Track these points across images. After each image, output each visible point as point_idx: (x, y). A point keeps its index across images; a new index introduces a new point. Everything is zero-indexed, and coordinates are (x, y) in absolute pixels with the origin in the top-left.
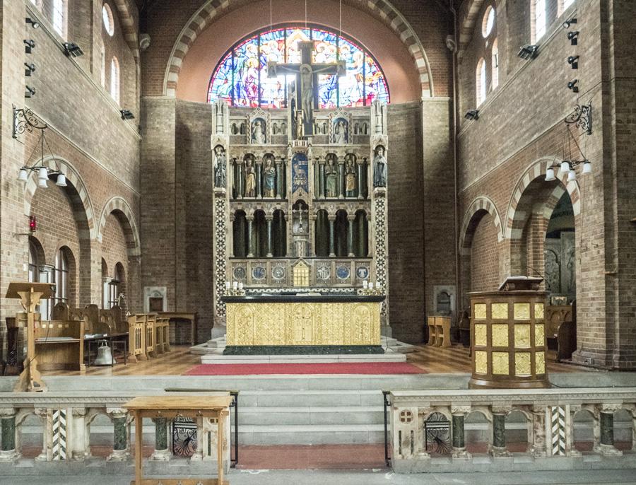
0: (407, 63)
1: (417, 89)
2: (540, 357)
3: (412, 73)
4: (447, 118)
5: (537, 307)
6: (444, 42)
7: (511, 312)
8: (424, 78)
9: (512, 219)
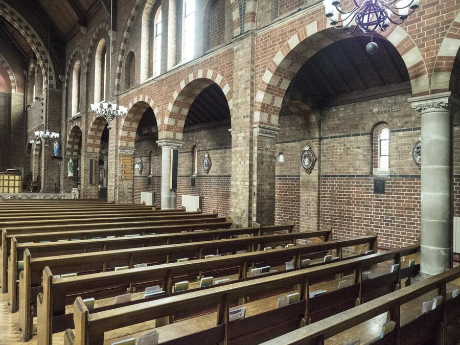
0: (6, 77)
1: (10, 88)
2: (17, 189)
3: (8, 82)
4: (23, 102)
5: (16, 177)
6: (23, 72)
7: (9, 177)
8: (13, 84)
9: (170, 111)
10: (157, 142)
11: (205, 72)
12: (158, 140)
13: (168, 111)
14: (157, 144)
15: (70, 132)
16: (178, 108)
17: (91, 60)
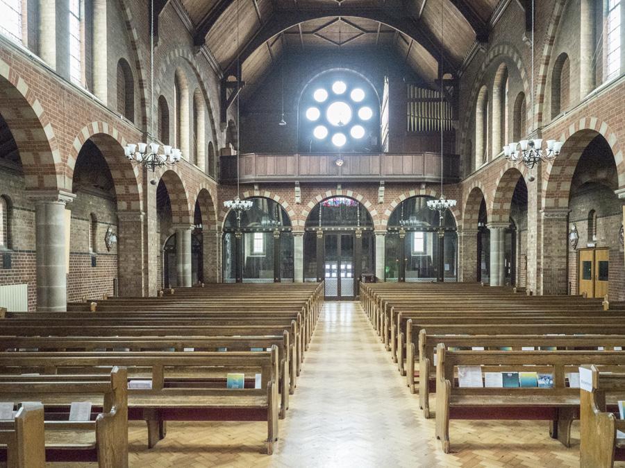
10: (616, 192)
11: (588, 122)
12: (618, 189)
13: (547, 173)
14: (617, 195)
15: (467, 197)
16: (502, 193)
17: (567, 12)
